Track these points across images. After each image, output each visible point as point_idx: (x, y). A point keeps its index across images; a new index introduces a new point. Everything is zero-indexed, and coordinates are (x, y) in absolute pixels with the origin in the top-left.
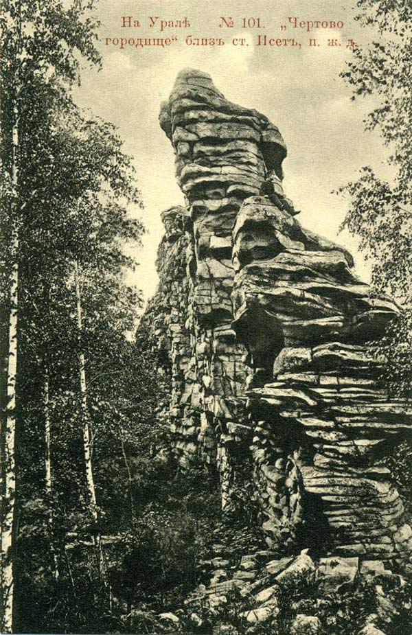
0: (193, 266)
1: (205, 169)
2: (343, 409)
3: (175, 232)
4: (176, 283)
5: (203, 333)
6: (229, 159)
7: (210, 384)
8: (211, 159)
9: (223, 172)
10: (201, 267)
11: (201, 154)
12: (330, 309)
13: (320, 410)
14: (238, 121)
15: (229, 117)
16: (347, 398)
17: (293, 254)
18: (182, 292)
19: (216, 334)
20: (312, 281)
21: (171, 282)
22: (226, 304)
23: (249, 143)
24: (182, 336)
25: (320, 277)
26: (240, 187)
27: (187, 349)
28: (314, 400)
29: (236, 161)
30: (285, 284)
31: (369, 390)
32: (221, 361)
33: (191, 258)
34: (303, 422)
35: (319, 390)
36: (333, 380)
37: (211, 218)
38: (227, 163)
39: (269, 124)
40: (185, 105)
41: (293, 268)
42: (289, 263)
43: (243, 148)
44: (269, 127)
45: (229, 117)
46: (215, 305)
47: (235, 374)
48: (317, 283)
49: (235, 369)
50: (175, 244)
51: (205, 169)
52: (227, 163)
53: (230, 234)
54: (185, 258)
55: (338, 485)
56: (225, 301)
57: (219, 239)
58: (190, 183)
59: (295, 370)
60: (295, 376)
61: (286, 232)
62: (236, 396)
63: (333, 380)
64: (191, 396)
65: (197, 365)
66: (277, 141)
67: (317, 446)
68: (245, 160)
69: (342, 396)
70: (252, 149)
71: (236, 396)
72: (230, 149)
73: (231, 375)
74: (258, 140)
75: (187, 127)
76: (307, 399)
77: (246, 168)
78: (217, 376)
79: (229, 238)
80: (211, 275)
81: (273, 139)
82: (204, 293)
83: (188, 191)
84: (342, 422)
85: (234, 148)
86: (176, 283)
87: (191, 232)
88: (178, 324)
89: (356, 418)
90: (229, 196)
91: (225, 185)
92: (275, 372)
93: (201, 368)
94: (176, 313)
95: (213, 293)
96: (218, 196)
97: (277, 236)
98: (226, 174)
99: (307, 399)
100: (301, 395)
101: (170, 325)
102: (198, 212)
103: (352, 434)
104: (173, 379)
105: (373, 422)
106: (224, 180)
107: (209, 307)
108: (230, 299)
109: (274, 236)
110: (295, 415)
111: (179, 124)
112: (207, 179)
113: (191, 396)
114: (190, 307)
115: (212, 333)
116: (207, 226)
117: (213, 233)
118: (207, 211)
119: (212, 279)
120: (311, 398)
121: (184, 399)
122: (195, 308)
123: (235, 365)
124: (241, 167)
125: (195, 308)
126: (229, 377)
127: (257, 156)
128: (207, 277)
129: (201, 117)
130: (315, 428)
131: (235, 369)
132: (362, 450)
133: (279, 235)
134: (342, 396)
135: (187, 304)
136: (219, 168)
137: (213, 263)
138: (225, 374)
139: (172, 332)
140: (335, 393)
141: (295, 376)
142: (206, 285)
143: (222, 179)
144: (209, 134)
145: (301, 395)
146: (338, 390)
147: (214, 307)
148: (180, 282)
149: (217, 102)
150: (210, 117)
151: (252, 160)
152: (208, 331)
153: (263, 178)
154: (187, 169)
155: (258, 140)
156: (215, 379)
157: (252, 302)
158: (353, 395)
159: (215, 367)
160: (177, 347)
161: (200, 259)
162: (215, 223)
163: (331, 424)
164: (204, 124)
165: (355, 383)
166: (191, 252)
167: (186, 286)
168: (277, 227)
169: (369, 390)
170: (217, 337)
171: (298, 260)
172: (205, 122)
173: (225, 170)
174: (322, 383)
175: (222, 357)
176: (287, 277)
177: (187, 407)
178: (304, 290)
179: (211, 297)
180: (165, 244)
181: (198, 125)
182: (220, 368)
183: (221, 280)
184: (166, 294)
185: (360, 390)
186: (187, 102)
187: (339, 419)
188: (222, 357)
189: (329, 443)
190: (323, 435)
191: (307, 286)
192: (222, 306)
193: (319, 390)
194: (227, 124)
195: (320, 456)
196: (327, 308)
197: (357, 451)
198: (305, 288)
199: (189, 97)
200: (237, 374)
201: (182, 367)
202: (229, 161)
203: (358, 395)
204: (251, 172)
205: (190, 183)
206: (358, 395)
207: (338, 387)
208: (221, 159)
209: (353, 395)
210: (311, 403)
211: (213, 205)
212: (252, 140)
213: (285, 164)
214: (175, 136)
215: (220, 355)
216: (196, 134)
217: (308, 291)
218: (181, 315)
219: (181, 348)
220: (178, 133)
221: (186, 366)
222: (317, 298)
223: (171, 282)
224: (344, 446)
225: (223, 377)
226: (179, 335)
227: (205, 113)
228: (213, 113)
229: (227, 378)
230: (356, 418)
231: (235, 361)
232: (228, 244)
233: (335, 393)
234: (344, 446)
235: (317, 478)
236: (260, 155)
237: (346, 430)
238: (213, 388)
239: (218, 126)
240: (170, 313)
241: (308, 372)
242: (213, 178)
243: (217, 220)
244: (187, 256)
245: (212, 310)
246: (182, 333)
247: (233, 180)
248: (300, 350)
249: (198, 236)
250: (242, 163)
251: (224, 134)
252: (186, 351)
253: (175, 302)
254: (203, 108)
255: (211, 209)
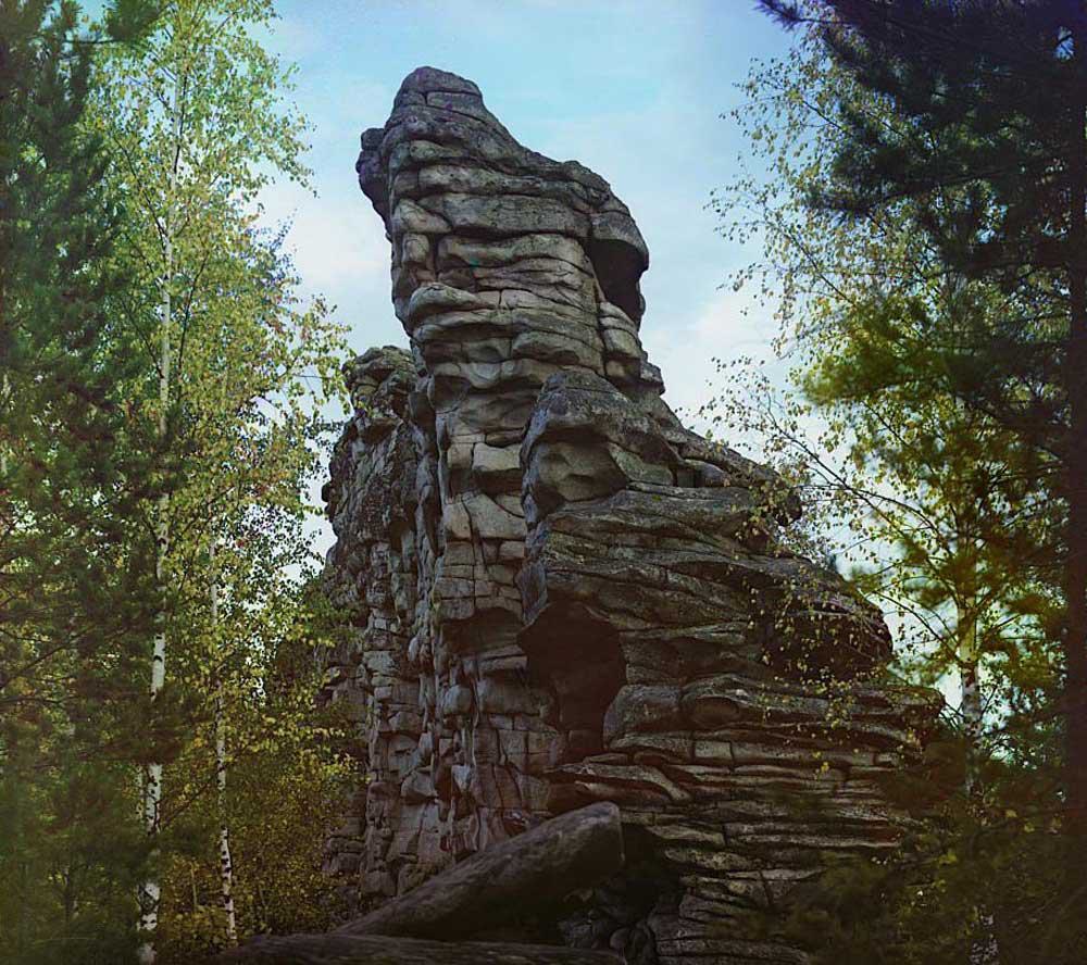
0: (434, 508)
1: (463, 295)
2: (743, 807)
3: (380, 416)
4: (383, 547)
5: (454, 665)
6: (516, 276)
7: (468, 781)
8: (479, 273)
9: (503, 304)
10: (452, 516)
11: (456, 262)
12: (720, 607)
13: (695, 809)
14: (538, 194)
15: (519, 183)
16: (750, 786)
17: (646, 492)
18: (401, 570)
19: (484, 666)
20: (684, 550)
21: (369, 544)
22: (507, 598)
23: (562, 238)
24: (397, 681)
25: (701, 541)
26: (541, 338)
27: (410, 715)
28: (682, 788)
29: (531, 278)
30: (629, 553)
31: (793, 771)
32: (496, 730)
33: (427, 490)
34: (659, 831)
35: (693, 769)
36: (722, 750)
37: (474, 404)
38: (513, 284)
39: (607, 199)
40: (421, 157)
41: (646, 523)
42: (640, 512)
43: (549, 252)
44: (609, 206)
45: (519, 183)
46: (482, 600)
47: (527, 759)
48: (698, 551)
49: (527, 746)
50: (381, 449)
51: (463, 295)
52: (513, 284)
53: (520, 490)
54: (414, 485)
55: (727, 955)
56: (505, 591)
57: (495, 452)
58: (428, 327)
59: (644, 728)
60: (643, 740)
61: (633, 447)
62: (527, 808)
63: (722, 750)
64: (418, 835)
65: (436, 749)
66: (625, 237)
67: (687, 879)
68: (553, 279)
69: (740, 781)
70: (570, 253)
71: (527, 808)
72: (520, 253)
73: (517, 760)
74: (583, 233)
75: (424, 202)
76: (669, 787)
77: (557, 296)
78: (483, 763)
79: (515, 450)
80: (475, 532)
81: (617, 234)
82: (459, 571)
83: (425, 343)
84: (739, 834)
85: (529, 251)
86: (383, 547)
87: (430, 430)
88: (385, 653)
89: (766, 825)
90: (517, 356)
91: (509, 332)
92: (606, 734)
93: (446, 755)
94: (381, 623)
95: (479, 572)
96: (495, 358)
97: (614, 455)
98: (511, 309)
99: (669, 787)
100: (656, 778)
101: (366, 654)
102: (450, 388)
103: (760, 856)
104: (370, 796)
105: (799, 833)
106: (506, 321)
107: (470, 604)
108: (515, 586)
109: (607, 454)
110: (644, 818)
111: (406, 195)
112: (467, 317)
113: (418, 835)
114: (421, 607)
115: (476, 664)
116: (467, 418)
117: (479, 438)
118: (466, 388)
119: (476, 539)
120: (675, 786)
121: (401, 844)
122: (437, 606)
123: (526, 740)
124: (544, 292)
125: (437, 606)
126: (512, 765)
127: (580, 269)
128: (468, 534)
129: (457, 181)
130: (683, 844)
131: (527, 746)
132: (778, 892)
133: (619, 455)
134: (740, 781)
135: (414, 600)
136: (497, 293)
137: (483, 504)
138: (503, 757)
139: (370, 673)
140: (726, 775)
141: (643, 740)
142: (465, 554)
143: (501, 318)
144: (472, 218)
145: (656, 778)
146: (732, 770)
147: (481, 603)
148: (396, 548)
149: (491, 149)
150: (476, 183)
151: (568, 279)
152: (466, 660)
153: (593, 317)
154: (420, 295)
155: (583, 233)
156: (481, 772)
157: (923, 597)
158: (762, 780)
159: (481, 742)
160: (384, 709)
161: (451, 494)
162: (484, 415)
163: (717, 838)
164: (463, 196)
165: (767, 755)
166: (429, 478)
167: (411, 555)
168: (614, 436)
169: (793, 771)
170: (487, 675)
171: (658, 506)
172: (466, 193)
173: (509, 297)
174: (700, 753)
175: (496, 720)
176: (633, 540)
177: (407, 866)
178: (666, 567)
179: (474, 580)
180: (354, 445)
181: (450, 198)
182: (494, 745)
183: (498, 542)
184: (355, 575)
185: (778, 769)
186: (423, 148)
187: (732, 827)
188: (496, 720)
189: (711, 872)
190: (698, 858)
191: (672, 559)
192: (500, 602)
193: (693, 769)
194: (514, 198)
195: (691, 898)
196: (714, 605)
197: (768, 892)
198: (669, 563)
199: (431, 137)
200: (532, 759)
201: (393, 763)
202: (518, 281)
203: (772, 780)
204: (565, 303)
205: (428, 327)
206: (772, 780)
207: (734, 763)
208: (500, 274)
209: (762, 780)
210: (676, 793)
211: (481, 374)
212: (568, 234)
213: (647, 283)
214: (397, 216)
215: (493, 714)
216: (445, 219)
217: (674, 569)
218: (393, 628)
219: (395, 713)
220: (407, 212)
221: (404, 759)
222: (693, 584)
223: (369, 544)
224: (739, 879)
225: (500, 766)
226: (390, 681)
227: (465, 174)
228: (484, 173)
229: (509, 766)
230: (766, 825)
231: (529, 729)
232: (514, 463)
233: (726, 775)
234: (739, 879)
235: (685, 939)
236: (589, 266)
237: (748, 850)
238: (476, 792)
239: (494, 203)
240: (366, 625)
241: (670, 734)
242: (482, 316)
243: (491, 406)
244: (420, 483)
245: (477, 611)
246: (396, 675)
247: (526, 320)
248: (657, 690)
249: (447, 442)
250: (549, 285)
251: (507, 220)
252: (406, 721)
253: (381, 597)
254: (465, 161)
255: (477, 383)
